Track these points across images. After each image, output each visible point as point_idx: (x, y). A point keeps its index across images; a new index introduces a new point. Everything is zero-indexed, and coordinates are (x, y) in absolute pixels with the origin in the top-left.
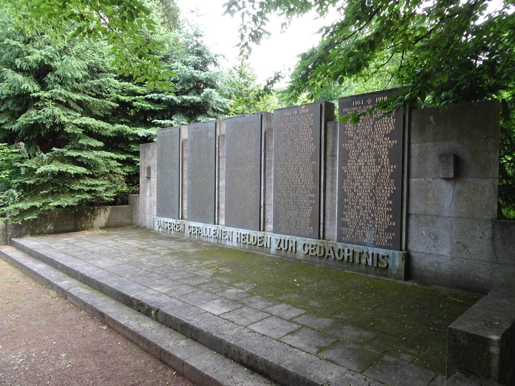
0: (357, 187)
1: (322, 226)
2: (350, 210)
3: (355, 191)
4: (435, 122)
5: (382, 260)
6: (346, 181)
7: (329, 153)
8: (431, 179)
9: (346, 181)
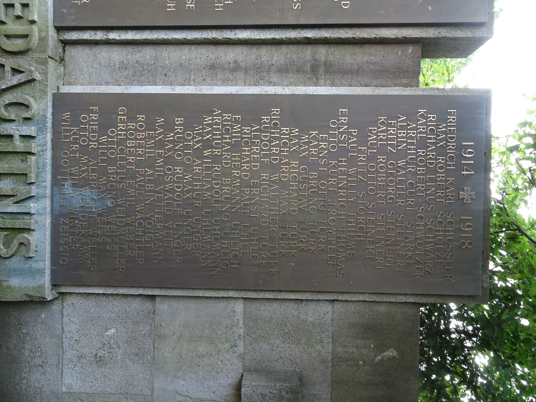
0: (217, 159)
1: (99, 35)
2: (150, 137)
3: (206, 153)
4: (382, 360)
5: (16, 243)
6: (236, 121)
7: (323, 53)
8: (241, 349)
9: (236, 121)
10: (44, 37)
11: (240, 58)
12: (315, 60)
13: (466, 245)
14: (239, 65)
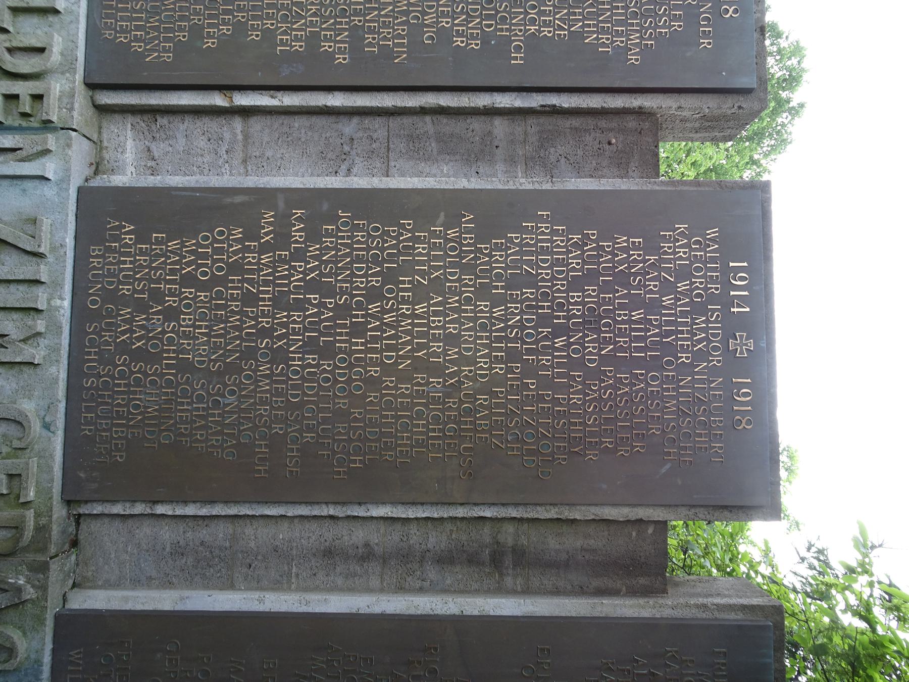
10: (44, 526)
11: (374, 539)
12: (498, 543)
13: (743, 424)
14: (373, 549)
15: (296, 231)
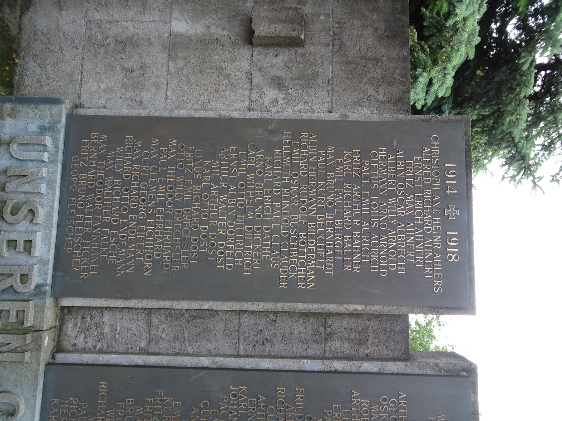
15: (214, 190)
